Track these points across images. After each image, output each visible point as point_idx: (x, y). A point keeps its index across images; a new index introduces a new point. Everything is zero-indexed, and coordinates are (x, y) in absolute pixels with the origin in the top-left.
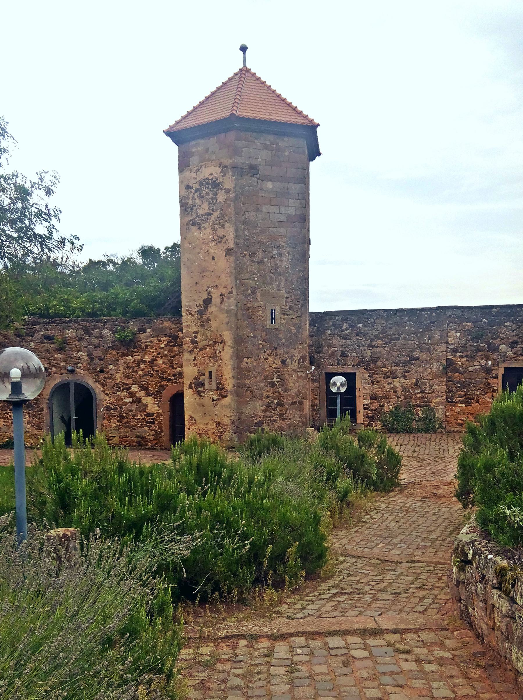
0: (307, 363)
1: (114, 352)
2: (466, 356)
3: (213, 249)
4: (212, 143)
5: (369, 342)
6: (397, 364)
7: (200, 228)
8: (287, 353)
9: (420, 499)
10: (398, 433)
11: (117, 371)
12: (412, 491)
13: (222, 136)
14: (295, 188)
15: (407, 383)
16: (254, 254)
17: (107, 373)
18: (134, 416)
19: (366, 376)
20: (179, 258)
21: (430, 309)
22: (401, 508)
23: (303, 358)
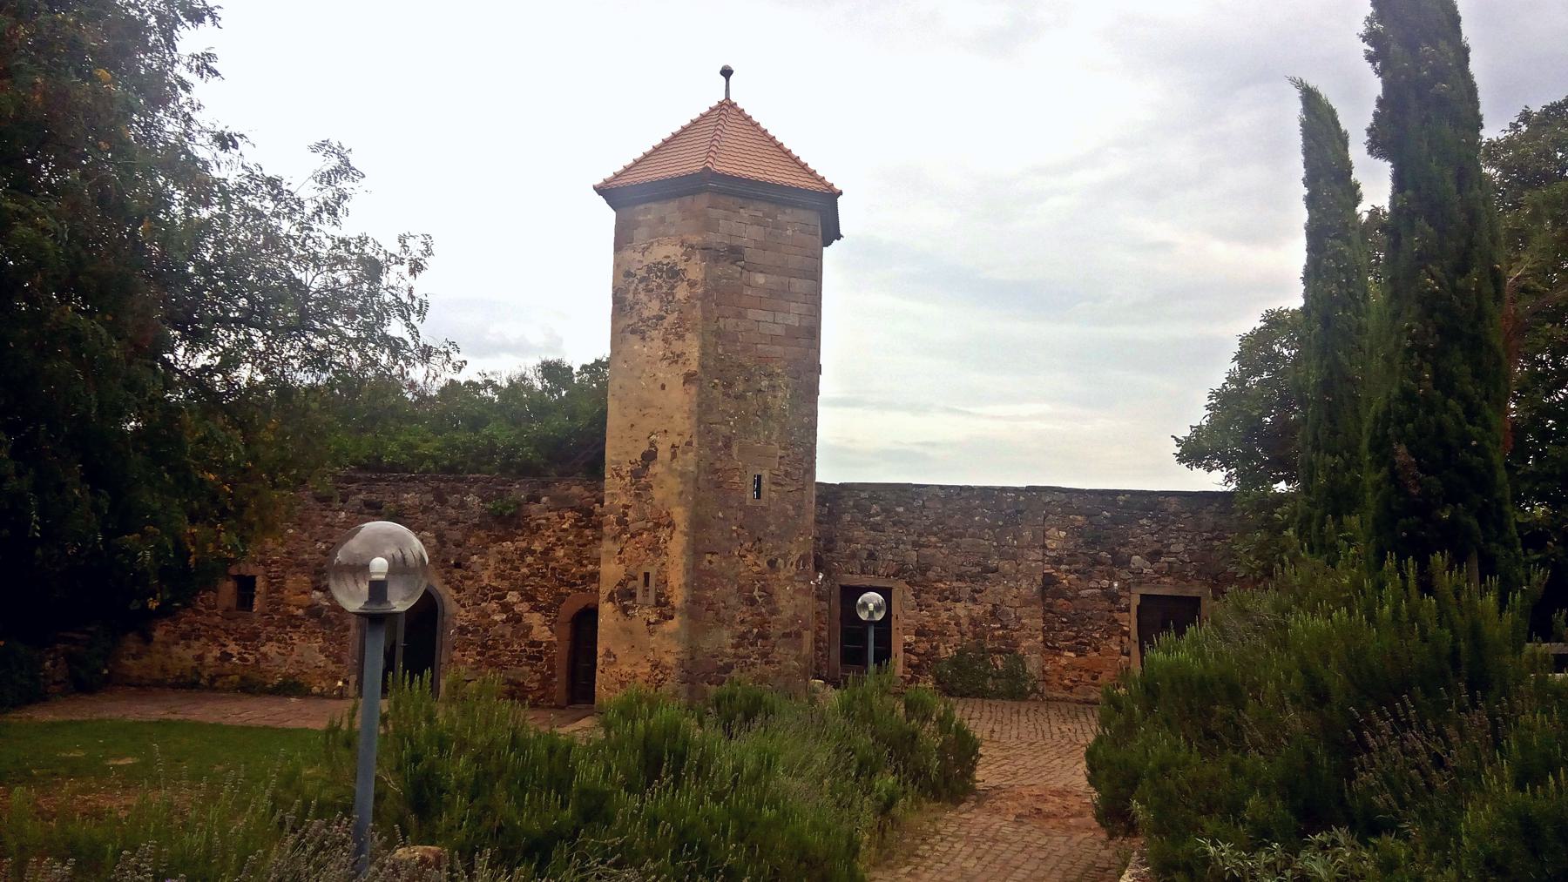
0: (811, 567)
1: (482, 534)
2: (1076, 571)
3: (664, 372)
4: (671, 210)
5: (915, 537)
6: (960, 578)
7: (643, 339)
8: (778, 548)
9: (1012, 818)
10: (962, 696)
11: (485, 566)
12: (999, 804)
13: (688, 199)
14: (800, 285)
15: (978, 610)
16: (730, 385)
17: (467, 568)
18: (507, 645)
19: (909, 595)
20: (606, 383)
21: (1016, 489)
22: (982, 835)
23: (804, 558)
